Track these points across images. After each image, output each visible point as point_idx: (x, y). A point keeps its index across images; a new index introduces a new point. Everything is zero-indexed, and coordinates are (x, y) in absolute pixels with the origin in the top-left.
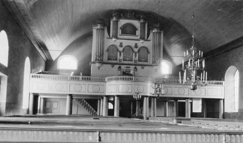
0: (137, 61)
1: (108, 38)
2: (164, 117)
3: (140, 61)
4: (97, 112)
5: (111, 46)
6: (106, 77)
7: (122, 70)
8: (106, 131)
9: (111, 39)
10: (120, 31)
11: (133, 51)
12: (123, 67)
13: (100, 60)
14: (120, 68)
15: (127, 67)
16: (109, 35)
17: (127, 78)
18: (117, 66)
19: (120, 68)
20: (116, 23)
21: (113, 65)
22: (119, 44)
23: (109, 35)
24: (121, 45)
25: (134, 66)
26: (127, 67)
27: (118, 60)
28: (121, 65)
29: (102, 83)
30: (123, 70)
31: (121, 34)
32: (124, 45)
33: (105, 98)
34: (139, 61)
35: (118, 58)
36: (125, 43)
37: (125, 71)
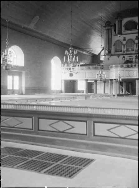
0: (126, 51)
1: (115, 35)
2: (87, 122)
3: (116, 52)
4: (123, 87)
5: (116, 41)
6: (109, 66)
7: (126, 59)
8: (30, 129)
9: (117, 35)
10: (123, 28)
11: (122, 43)
12: (126, 57)
13: (108, 53)
14: (124, 57)
15: (129, 57)
16: (116, 33)
17: (127, 65)
18: (122, 57)
19: (124, 57)
20: (120, 22)
21: (118, 56)
22: (135, 37)
23: (116, 33)
24: (124, 39)
25: (135, 55)
26: (129, 57)
27: (135, 51)
28: (125, 56)
29: (108, 71)
30: (127, 58)
31: (124, 30)
32: (127, 39)
33: (109, 81)
34: (127, 51)
35: (122, 50)
36: (128, 37)
37: (128, 59)
